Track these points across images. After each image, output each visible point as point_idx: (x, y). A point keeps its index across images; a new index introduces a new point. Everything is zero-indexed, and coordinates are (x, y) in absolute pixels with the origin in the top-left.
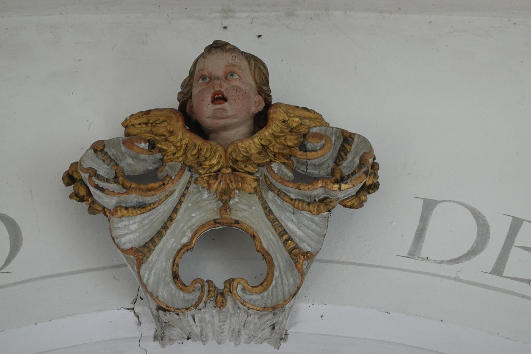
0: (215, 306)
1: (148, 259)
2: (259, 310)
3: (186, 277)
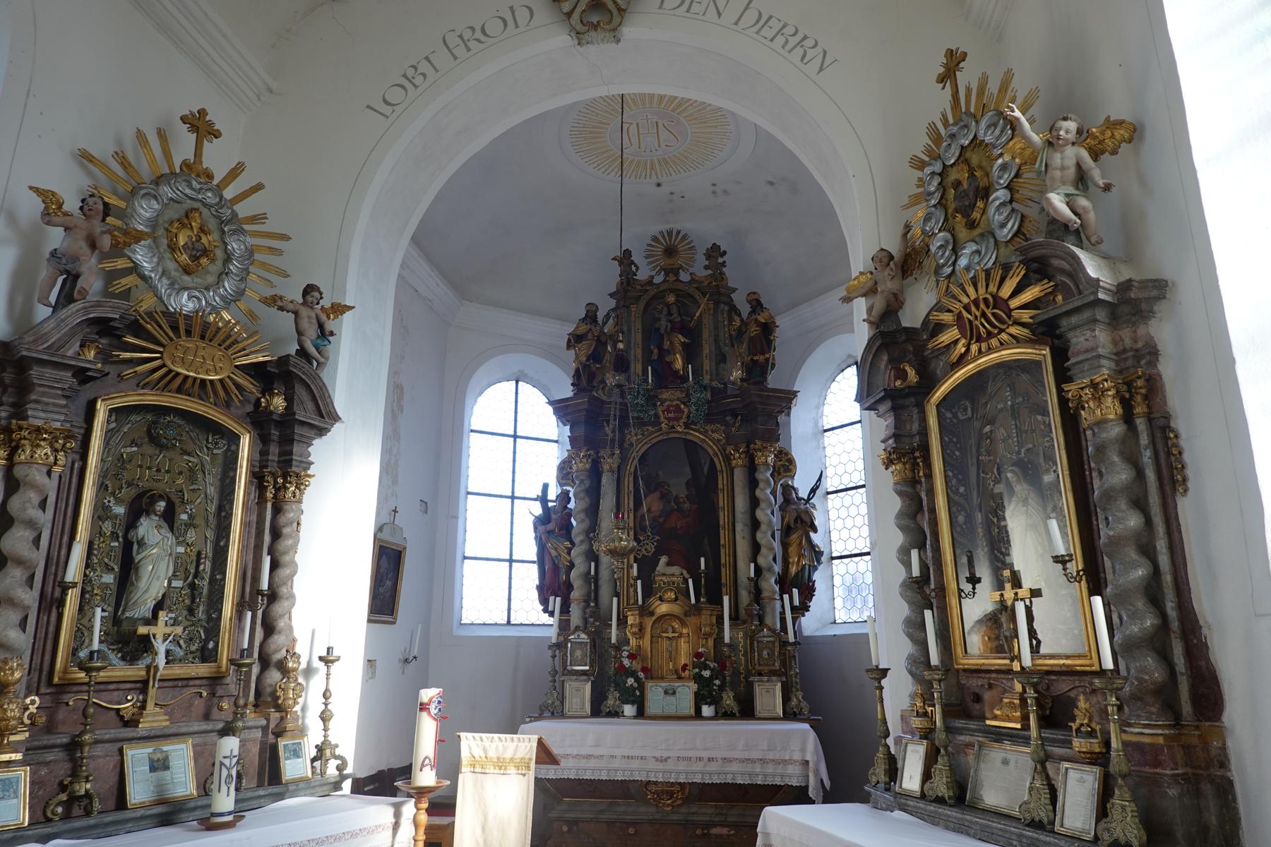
0: (894, 254)
1: (952, 370)
2: (945, 197)
3: (585, 22)
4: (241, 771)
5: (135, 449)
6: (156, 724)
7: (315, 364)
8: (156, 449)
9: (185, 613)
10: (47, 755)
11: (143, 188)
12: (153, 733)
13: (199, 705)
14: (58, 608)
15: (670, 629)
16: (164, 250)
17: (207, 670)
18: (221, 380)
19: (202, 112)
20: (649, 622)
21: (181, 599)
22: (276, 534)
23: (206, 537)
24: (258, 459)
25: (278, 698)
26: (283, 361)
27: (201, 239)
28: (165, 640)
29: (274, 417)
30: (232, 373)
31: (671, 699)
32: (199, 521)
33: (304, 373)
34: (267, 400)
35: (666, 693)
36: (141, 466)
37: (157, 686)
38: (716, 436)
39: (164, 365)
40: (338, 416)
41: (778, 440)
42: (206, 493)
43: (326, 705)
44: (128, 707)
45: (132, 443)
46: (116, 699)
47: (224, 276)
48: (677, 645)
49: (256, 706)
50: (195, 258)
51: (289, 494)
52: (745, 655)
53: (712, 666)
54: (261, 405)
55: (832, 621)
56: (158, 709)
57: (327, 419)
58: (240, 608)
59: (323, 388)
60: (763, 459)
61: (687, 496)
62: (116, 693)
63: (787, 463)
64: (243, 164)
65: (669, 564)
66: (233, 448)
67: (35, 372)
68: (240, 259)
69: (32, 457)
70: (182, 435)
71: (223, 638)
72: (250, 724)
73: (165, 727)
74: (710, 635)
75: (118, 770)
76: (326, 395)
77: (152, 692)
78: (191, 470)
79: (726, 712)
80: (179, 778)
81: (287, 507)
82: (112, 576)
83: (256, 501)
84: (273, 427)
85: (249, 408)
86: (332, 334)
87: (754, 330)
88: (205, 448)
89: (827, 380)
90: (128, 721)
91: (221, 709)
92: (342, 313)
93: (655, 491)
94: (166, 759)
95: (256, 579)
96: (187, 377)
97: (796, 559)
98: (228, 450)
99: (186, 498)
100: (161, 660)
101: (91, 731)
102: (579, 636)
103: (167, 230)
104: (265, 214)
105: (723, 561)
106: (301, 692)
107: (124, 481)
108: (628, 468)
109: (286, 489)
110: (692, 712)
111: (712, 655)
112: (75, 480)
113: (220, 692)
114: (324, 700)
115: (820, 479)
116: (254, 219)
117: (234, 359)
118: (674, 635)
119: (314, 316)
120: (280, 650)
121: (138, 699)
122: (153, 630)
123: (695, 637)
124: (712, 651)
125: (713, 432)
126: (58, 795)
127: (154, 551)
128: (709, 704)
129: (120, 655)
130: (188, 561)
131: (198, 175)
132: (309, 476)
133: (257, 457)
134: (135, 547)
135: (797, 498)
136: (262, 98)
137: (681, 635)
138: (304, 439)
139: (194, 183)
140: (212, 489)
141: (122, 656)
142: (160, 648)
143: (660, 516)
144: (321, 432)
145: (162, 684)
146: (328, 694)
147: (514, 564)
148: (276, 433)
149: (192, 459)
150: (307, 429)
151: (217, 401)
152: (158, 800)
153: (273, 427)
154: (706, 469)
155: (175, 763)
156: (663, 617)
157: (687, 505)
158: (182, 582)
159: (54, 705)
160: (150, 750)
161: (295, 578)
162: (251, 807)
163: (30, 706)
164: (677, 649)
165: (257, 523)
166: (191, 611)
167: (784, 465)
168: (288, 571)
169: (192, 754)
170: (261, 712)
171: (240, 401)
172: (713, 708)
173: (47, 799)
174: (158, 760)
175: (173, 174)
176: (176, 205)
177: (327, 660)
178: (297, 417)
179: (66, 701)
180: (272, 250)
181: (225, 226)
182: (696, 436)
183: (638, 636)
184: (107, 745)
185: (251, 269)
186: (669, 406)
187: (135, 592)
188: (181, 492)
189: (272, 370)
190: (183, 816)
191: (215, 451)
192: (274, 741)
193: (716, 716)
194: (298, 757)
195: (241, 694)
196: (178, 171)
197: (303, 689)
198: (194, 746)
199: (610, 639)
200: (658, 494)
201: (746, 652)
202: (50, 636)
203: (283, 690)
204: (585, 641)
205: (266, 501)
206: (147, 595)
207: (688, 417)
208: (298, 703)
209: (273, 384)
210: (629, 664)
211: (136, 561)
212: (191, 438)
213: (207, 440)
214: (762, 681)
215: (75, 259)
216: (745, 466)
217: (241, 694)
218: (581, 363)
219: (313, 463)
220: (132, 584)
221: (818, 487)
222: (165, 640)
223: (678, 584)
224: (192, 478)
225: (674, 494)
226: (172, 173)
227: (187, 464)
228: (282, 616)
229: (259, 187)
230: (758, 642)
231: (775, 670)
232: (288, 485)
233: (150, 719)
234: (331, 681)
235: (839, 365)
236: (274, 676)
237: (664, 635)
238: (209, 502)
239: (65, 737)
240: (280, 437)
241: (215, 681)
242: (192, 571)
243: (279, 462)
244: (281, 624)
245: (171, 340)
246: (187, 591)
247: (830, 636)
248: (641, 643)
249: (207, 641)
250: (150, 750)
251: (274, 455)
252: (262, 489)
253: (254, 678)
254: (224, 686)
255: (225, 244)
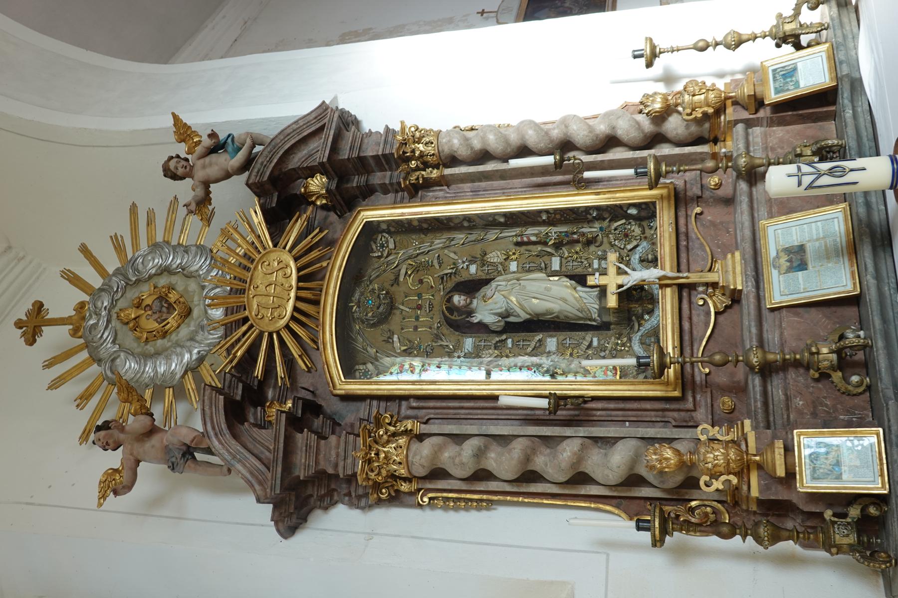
4: (814, 148)
5: (395, 338)
6: (738, 269)
7: (258, 149)
8: (394, 314)
9: (592, 248)
10: (776, 399)
11: (106, 375)
12: (751, 272)
13: (713, 214)
14: (585, 402)
16: (168, 341)
17: (666, 213)
18: (296, 259)
19: (19, 324)
21: (575, 256)
22: (484, 156)
23: (496, 239)
24: (393, 195)
25: (705, 114)
26: (257, 189)
27: (148, 305)
28: (626, 273)
29: (333, 186)
30: (284, 248)
32: (477, 250)
33: (270, 161)
34: (317, 198)
36: (416, 328)
37: (685, 275)
39: (270, 335)
40: (320, 106)
42: (442, 248)
43: (717, 44)
44: (714, 302)
45: (387, 342)
46: (702, 317)
47: (185, 272)
49: (715, 141)
50: (170, 308)
51: (430, 150)
54: (325, 204)
56: (718, 266)
57: (326, 120)
58: (583, 185)
59: (284, 134)
62: (695, 319)
64: (63, 271)
66: (384, 227)
67: (301, 473)
68: (164, 257)
69: (400, 463)
70: (373, 289)
71: (623, 198)
72: (741, 146)
73: (743, 257)
75: (800, 310)
76: (295, 127)
77: (694, 278)
78: (416, 270)
80: (817, 230)
81: (446, 150)
82: (549, 340)
83: (445, 187)
84: (349, 185)
85: (333, 217)
86: (213, 135)
88: (390, 258)
90: (732, 300)
91: (719, 186)
92: (187, 127)
94: (788, 251)
95: (544, 171)
96: (298, 298)
98: (389, 232)
99: (450, 271)
100: (651, 274)
101: (746, 353)
103: (147, 341)
104: (111, 237)
106: (697, 84)
107: (434, 344)
109: (422, 155)
112: (431, 404)
113: (696, 191)
114: (710, 49)
116: (118, 245)
117: (265, 248)
119: (202, 161)
120: (638, 123)
121: (703, 292)
122: (612, 289)
126: (833, 382)
127: (514, 299)
129: (646, 317)
130: (527, 256)
131: (83, 318)
132: (403, 129)
133: (390, 196)
134: (512, 319)
136: (21, 255)
138: (357, 144)
139: (91, 322)
140: (437, 241)
141: (648, 313)
142: (636, 278)
144: (347, 122)
145: (684, 266)
146: (701, 44)
148: (356, 180)
149: (403, 272)
150: (344, 142)
151: (328, 257)
152: (850, 254)
153: (349, 185)
155: (794, 239)
158: (553, 259)
159: (709, 390)
160: (775, 273)
161: (539, 120)
162: (869, 125)
163: (711, 434)
165: (473, 181)
166: (589, 242)
168: (531, 132)
169: (783, 217)
170: (725, 133)
171: (321, 231)
173: (838, 394)
174: (790, 261)
175: (87, 346)
176: (119, 337)
177: (651, 57)
178: (325, 160)
179: (704, 377)
180: (150, 222)
181: (130, 280)
184: (766, 327)
185: (174, 242)
187: (566, 313)
188: (442, 278)
189: (275, 199)
190: (876, 218)
191: (391, 246)
192: (768, 109)
194: (795, 69)
195: (699, 166)
196: (82, 341)
197: (694, 82)
198: (771, 216)
202: (621, 405)
203: (693, 110)
205: (443, 177)
206: (571, 299)
208: (714, 85)
209: (296, 194)
211: (528, 317)
212: (378, 276)
213: (379, 257)
215: (167, 449)
217: (699, 166)
219: (387, 126)
220: (557, 317)
222: (626, 273)
224: (427, 267)
226: (87, 347)
227: (410, 276)
228: (591, 129)
229: (84, 250)
232: (417, 154)
233: (731, 278)
234: (681, 44)
236: (674, 125)
238: (453, 243)
239: (753, 380)
240: (360, 174)
241: (679, 199)
242: (539, 248)
243: (391, 170)
244: (602, 128)
245: (251, 326)
246: (565, 251)
249: (629, 217)
250: (775, 273)
251: (385, 177)
252: (428, 184)
253: (677, 151)
254: (688, 186)
255: (150, 277)
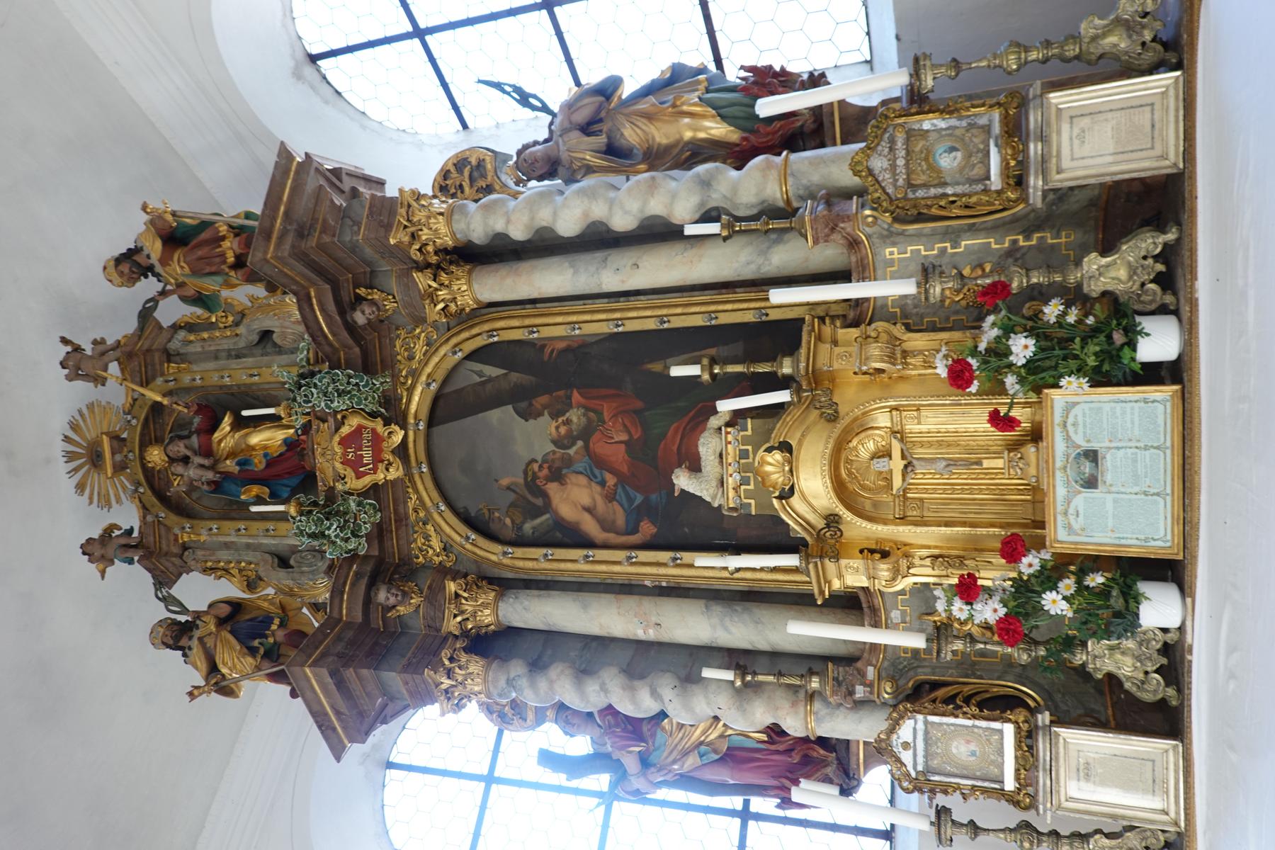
15: (881, 465)
20: (857, 529)
31: (1112, 466)
35: (1091, 483)
38: (419, 349)
41: (418, 196)
48: (930, 444)
52: (954, 236)
53: (995, 332)
55: (867, 67)
60: (440, 225)
61: (554, 416)
63: (466, 172)
65: (695, 467)
74: (894, 341)
79: (1158, 279)
87: (178, 267)
89: (364, 127)
93: (545, 495)
97: (687, 120)
102: (906, 745)
105: (698, 321)
108: (494, 558)
110: (1163, 394)
111: (956, 335)
115: (498, 86)
118: (896, 453)
123: (903, 388)
124: (945, 335)
125: (411, 358)
128: (1132, 336)
135: (546, 141)
137: (898, 433)
143: (603, 483)
147: (737, 821)
154: (492, 371)
156: (840, 488)
157: (575, 416)
164: (940, 444)
167: (472, 180)
172: (1146, 323)
182: (418, 402)
183: (904, 563)
186: (345, 462)
193: (1176, 313)
199: (916, 652)
200: (552, 488)
201: (948, 235)
204: (920, 726)
207: (373, 415)
210: (995, 603)
214: (1044, 160)
216: (470, 272)
218: (258, 668)
221: (518, 90)
223: (745, 441)
225: (552, 447)
230: (911, 185)
231: (1005, 119)
235: (327, 102)
237: (897, 482)
247: (899, 50)
248: (925, 552)
